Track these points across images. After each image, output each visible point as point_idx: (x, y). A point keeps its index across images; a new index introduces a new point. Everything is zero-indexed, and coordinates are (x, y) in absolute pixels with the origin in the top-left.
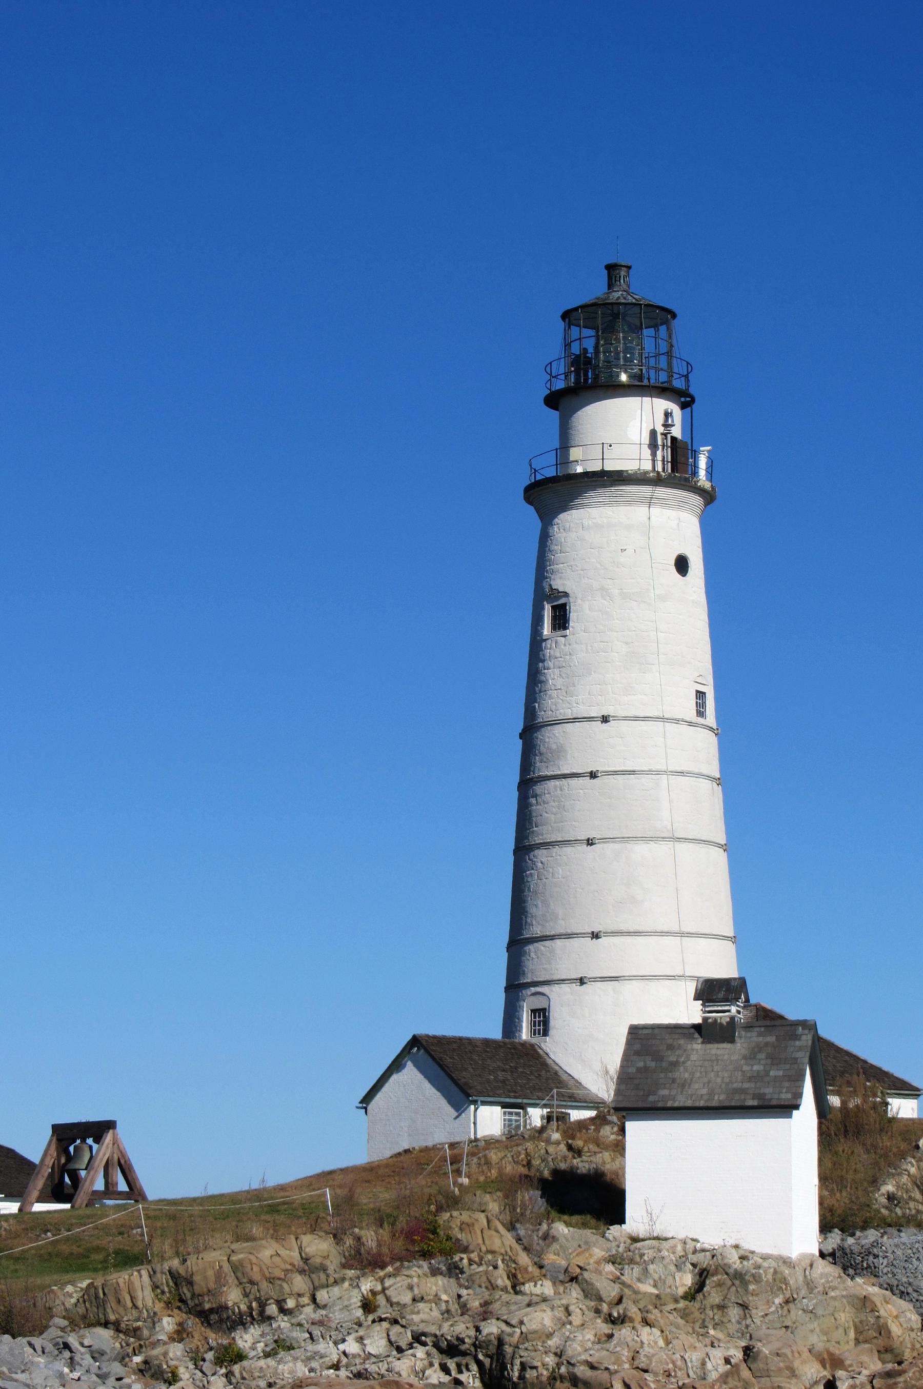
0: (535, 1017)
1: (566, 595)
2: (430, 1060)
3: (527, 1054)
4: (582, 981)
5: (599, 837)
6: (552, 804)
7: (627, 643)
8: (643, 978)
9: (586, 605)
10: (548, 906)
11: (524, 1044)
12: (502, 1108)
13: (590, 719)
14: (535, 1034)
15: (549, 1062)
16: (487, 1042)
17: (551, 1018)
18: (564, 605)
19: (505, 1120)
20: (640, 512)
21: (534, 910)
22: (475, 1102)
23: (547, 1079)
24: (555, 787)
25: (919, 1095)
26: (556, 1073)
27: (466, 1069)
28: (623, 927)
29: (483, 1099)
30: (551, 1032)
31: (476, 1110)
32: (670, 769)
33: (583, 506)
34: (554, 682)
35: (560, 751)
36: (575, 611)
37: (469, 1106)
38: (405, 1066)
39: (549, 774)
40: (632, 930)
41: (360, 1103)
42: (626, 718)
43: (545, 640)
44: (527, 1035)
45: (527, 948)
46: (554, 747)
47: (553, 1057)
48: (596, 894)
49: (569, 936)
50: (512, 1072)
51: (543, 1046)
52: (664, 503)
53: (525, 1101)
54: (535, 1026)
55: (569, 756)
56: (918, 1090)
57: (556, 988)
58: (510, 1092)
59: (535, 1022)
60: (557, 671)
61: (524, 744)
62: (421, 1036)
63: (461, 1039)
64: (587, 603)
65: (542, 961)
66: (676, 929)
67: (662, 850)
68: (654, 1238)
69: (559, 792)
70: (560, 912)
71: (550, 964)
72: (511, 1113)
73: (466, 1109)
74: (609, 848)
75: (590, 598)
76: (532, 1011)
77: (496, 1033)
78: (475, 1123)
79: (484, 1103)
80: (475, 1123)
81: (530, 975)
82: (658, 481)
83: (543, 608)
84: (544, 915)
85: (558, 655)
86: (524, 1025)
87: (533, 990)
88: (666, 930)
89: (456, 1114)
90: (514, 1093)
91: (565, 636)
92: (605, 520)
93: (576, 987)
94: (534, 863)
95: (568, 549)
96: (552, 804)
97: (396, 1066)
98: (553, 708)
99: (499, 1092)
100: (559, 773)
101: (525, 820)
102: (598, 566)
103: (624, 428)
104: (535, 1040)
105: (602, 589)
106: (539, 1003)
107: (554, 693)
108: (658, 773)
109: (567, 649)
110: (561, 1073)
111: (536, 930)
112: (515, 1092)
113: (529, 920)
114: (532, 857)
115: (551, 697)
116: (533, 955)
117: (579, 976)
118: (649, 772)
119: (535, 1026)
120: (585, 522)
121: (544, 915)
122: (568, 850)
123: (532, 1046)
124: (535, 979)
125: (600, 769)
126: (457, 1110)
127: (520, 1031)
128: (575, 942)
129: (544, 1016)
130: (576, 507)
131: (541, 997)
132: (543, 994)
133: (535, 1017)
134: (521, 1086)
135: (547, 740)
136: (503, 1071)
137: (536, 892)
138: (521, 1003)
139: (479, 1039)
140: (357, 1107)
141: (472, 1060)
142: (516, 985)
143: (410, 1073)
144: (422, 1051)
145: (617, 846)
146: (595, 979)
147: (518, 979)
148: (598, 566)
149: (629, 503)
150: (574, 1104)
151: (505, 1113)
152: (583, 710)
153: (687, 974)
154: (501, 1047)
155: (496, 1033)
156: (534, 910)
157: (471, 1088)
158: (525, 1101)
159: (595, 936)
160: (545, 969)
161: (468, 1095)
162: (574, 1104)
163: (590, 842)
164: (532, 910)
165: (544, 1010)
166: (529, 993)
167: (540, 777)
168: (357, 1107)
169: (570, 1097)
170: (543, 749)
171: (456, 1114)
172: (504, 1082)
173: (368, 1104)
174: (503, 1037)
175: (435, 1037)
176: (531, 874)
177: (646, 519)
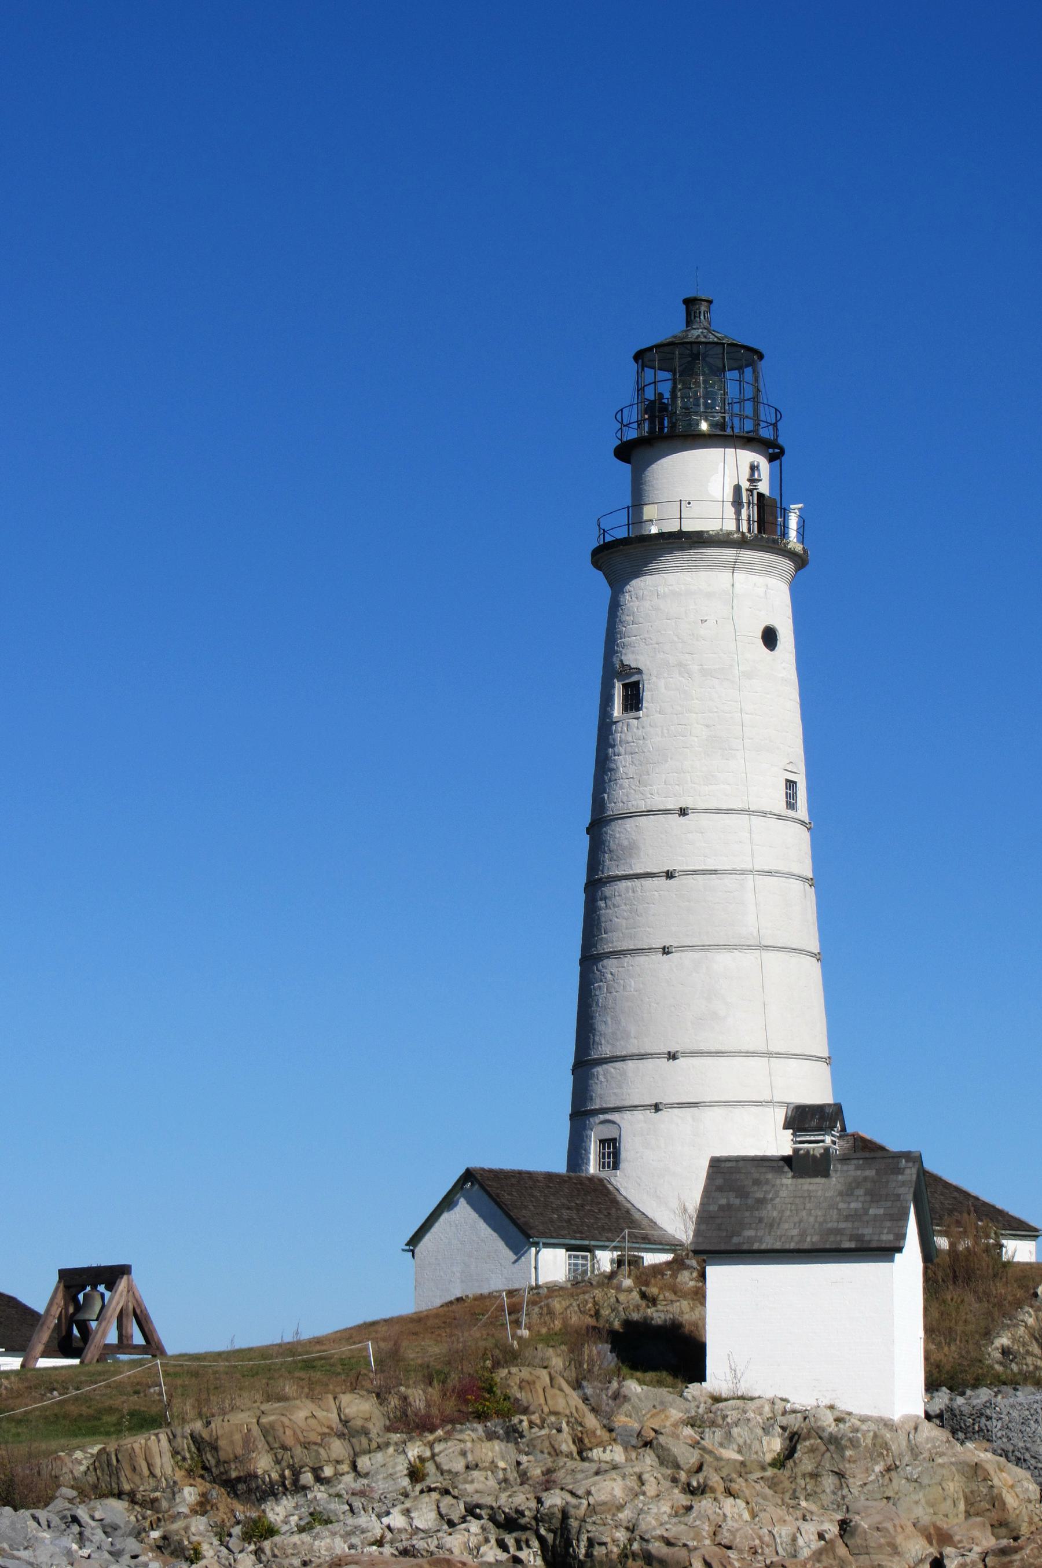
0: (604, 1149)
1: (639, 671)
2: (486, 1197)
3: (595, 1190)
4: (657, 1107)
5: (676, 945)
6: (624, 907)
7: (707, 726)
8: (726, 1104)
9: (661, 683)
10: (618, 1022)
11: (591, 1179)
12: (567, 1250)
13: (666, 812)
14: (604, 1167)
15: (620, 1198)
16: (550, 1177)
17: (622, 1149)
18: (637, 683)
19: (570, 1264)
20: (723, 577)
21: (603, 1027)
22: (536, 1244)
23: (618, 1218)
24: (627, 888)
25: (1037, 1236)
26: (628, 1211)
27: (526, 1207)
28: (703, 1047)
29: (545, 1240)
30: (622, 1165)
31: (537, 1253)
32: (757, 868)
33: (658, 571)
34: (625, 770)
35: (632, 848)
36: (649, 690)
37: (529, 1248)
38: (457, 1203)
39: (620, 873)
40: (713, 1050)
41: (407, 1245)
42: (707, 811)
43: (616, 723)
44: (595, 1168)
45: (595, 1070)
46: (626, 843)
47: (624, 1194)
48: (673, 1009)
49: (642, 1057)
50: (578, 1210)
51: (613, 1180)
52: (749, 568)
53: (593, 1243)
54: (604, 1158)
55: (642, 854)
56: (1036, 1230)
57: (627, 1115)
58: (575, 1232)
59: (604, 1154)
60: (628, 758)
61: (592, 840)
62: (475, 1170)
63: (520, 1173)
64: (663, 681)
65: (612, 1085)
66: (764, 1049)
67: (747, 959)
68: (739, 1398)
69: (631, 894)
70: (633, 1030)
71: (621, 1088)
72: (576, 1257)
73: (526, 1252)
74: (688, 957)
75: (666, 675)
76: (601, 1141)
77: (560, 1166)
78: (536, 1268)
79: (547, 1245)
80: (536, 1268)
81: (598, 1101)
82: (742, 543)
83: (613, 687)
84: (614, 1033)
85: (630, 739)
86: (592, 1157)
87: (602, 1117)
88: (752, 1049)
89: (515, 1257)
90: (580, 1233)
91: (638, 718)
92: (683, 587)
93: (650, 1114)
94: (603, 974)
95: (641, 620)
96: (624, 907)
97: (447, 1203)
98: (625, 799)
99: (563, 1232)
100: (631, 872)
101: (593, 925)
102: (676, 639)
103: (704, 483)
104: (604, 1174)
105: (680, 665)
106: (608, 1132)
107: (625, 783)
108: (743, 872)
109: (640, 733)
110: (633, 1211)
111: (605, 1049)
112: (581, 1233)
113: (597, 1039)
114: (600, 967)
115: (622, 787)
116: (601, 1078)
117: (654, 1102)
118: (733, 872)
119: (604, 1158)
120: (661, 590)
121: (614, 1033)
122: (642, 959)
123: (601, 1180)
124: (604, 1106)
125: (678, 868)
126: (516, 1254)
127: (588, 1164)
128: (649, 1063)
129: (615, 1147)
130: (650, 573)
131: (610, 1126)
132: (614, 1122)
133: (604, 1149)
134: (588, 1226)
135: (618, 835)
136: (568, 1208)
137: (605, 1007)
138: (589, 1132)
139: (541, 1173)
140: (403, 1250)
141: (533, 1196)
142: (582, 1112)
143: (463, 1211)
144: (477, 1186)
145: (696, 955)
146: (672, 1106)
147: (585, 1106)
148: (676, 639)
149: (710, 568)
150: (648, 1246)
151: (570, 1257)
152: (658, 802)
153: (775, 1100)
154: (565, 1181)
155: (560, 1166)
156: (603, 1027)
157: (531, 1228)
158: (593, 1243)
159: (672, 1056)
160: (615, 1094)
161: (528, 1236)
162: (648, 1246)
163: (666, 951)
164: (601, 1027)
165: (614, 1141)
166: (597, 1121)
167: (609, 877)
168: (403, 1250)
169: (643, 1238)
170: (613, 846)
171: (515, 1257)
172: (569, 1221)
173: (415, 1246)
174: (568, 1171)
175: (491, 1171)
176: (600, 987)
177: (729, 586)
